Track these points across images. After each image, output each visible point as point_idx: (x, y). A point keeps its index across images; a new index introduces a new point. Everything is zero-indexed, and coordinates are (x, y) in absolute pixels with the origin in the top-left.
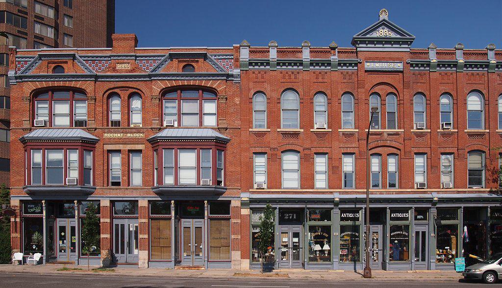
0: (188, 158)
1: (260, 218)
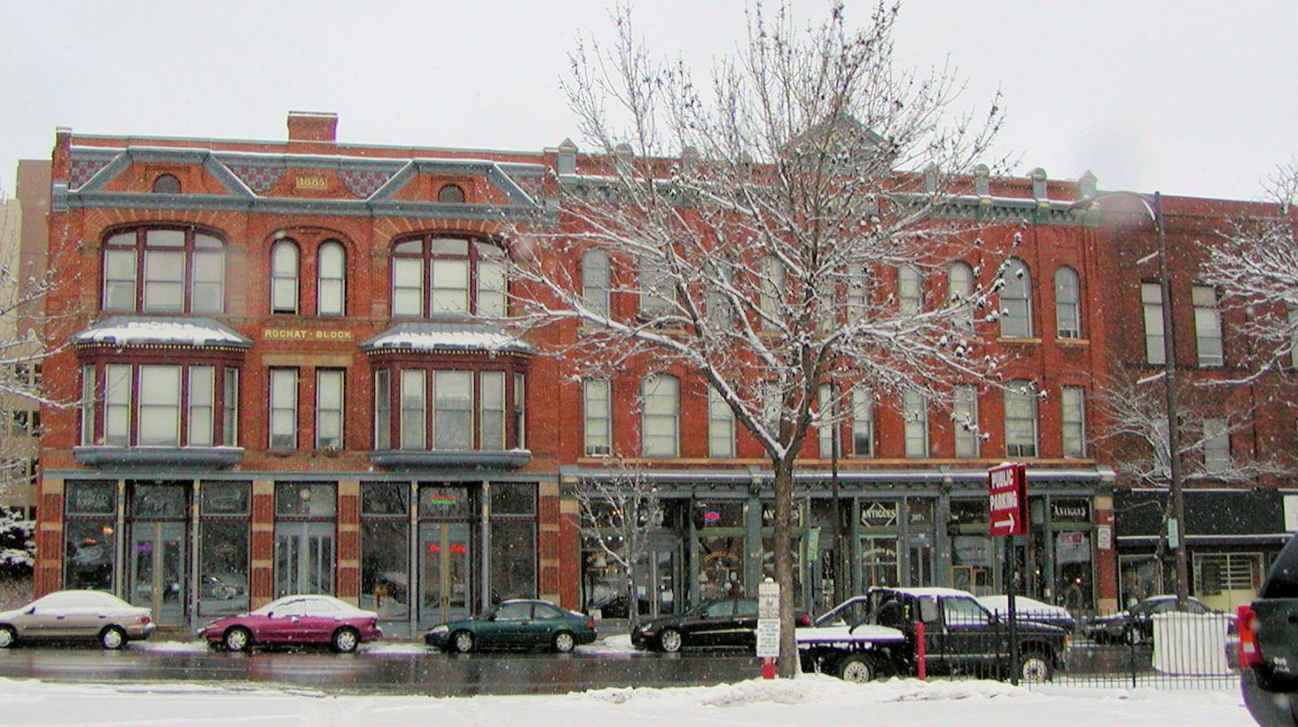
0: (160, 383)
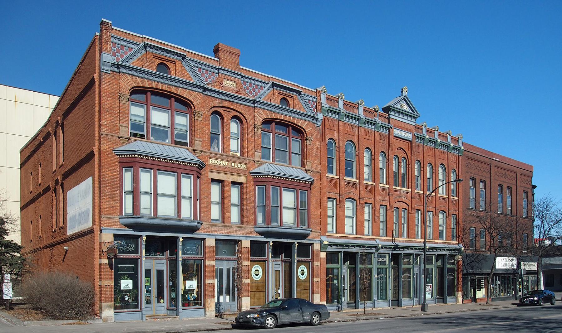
1: (525, 265)
